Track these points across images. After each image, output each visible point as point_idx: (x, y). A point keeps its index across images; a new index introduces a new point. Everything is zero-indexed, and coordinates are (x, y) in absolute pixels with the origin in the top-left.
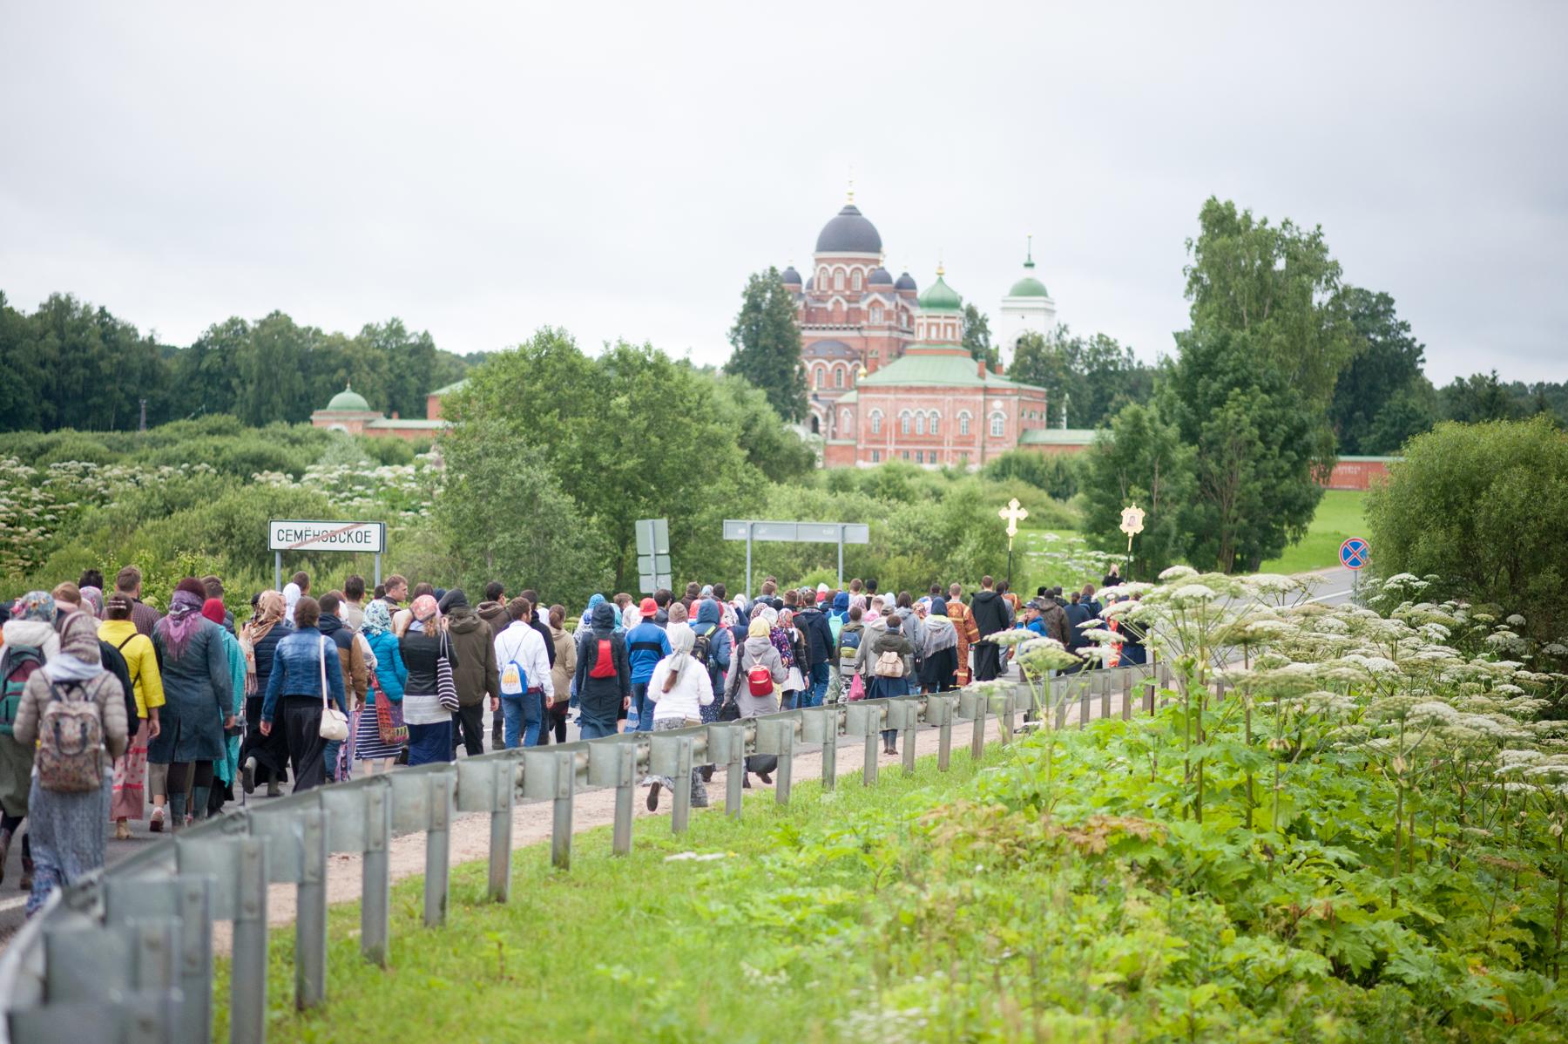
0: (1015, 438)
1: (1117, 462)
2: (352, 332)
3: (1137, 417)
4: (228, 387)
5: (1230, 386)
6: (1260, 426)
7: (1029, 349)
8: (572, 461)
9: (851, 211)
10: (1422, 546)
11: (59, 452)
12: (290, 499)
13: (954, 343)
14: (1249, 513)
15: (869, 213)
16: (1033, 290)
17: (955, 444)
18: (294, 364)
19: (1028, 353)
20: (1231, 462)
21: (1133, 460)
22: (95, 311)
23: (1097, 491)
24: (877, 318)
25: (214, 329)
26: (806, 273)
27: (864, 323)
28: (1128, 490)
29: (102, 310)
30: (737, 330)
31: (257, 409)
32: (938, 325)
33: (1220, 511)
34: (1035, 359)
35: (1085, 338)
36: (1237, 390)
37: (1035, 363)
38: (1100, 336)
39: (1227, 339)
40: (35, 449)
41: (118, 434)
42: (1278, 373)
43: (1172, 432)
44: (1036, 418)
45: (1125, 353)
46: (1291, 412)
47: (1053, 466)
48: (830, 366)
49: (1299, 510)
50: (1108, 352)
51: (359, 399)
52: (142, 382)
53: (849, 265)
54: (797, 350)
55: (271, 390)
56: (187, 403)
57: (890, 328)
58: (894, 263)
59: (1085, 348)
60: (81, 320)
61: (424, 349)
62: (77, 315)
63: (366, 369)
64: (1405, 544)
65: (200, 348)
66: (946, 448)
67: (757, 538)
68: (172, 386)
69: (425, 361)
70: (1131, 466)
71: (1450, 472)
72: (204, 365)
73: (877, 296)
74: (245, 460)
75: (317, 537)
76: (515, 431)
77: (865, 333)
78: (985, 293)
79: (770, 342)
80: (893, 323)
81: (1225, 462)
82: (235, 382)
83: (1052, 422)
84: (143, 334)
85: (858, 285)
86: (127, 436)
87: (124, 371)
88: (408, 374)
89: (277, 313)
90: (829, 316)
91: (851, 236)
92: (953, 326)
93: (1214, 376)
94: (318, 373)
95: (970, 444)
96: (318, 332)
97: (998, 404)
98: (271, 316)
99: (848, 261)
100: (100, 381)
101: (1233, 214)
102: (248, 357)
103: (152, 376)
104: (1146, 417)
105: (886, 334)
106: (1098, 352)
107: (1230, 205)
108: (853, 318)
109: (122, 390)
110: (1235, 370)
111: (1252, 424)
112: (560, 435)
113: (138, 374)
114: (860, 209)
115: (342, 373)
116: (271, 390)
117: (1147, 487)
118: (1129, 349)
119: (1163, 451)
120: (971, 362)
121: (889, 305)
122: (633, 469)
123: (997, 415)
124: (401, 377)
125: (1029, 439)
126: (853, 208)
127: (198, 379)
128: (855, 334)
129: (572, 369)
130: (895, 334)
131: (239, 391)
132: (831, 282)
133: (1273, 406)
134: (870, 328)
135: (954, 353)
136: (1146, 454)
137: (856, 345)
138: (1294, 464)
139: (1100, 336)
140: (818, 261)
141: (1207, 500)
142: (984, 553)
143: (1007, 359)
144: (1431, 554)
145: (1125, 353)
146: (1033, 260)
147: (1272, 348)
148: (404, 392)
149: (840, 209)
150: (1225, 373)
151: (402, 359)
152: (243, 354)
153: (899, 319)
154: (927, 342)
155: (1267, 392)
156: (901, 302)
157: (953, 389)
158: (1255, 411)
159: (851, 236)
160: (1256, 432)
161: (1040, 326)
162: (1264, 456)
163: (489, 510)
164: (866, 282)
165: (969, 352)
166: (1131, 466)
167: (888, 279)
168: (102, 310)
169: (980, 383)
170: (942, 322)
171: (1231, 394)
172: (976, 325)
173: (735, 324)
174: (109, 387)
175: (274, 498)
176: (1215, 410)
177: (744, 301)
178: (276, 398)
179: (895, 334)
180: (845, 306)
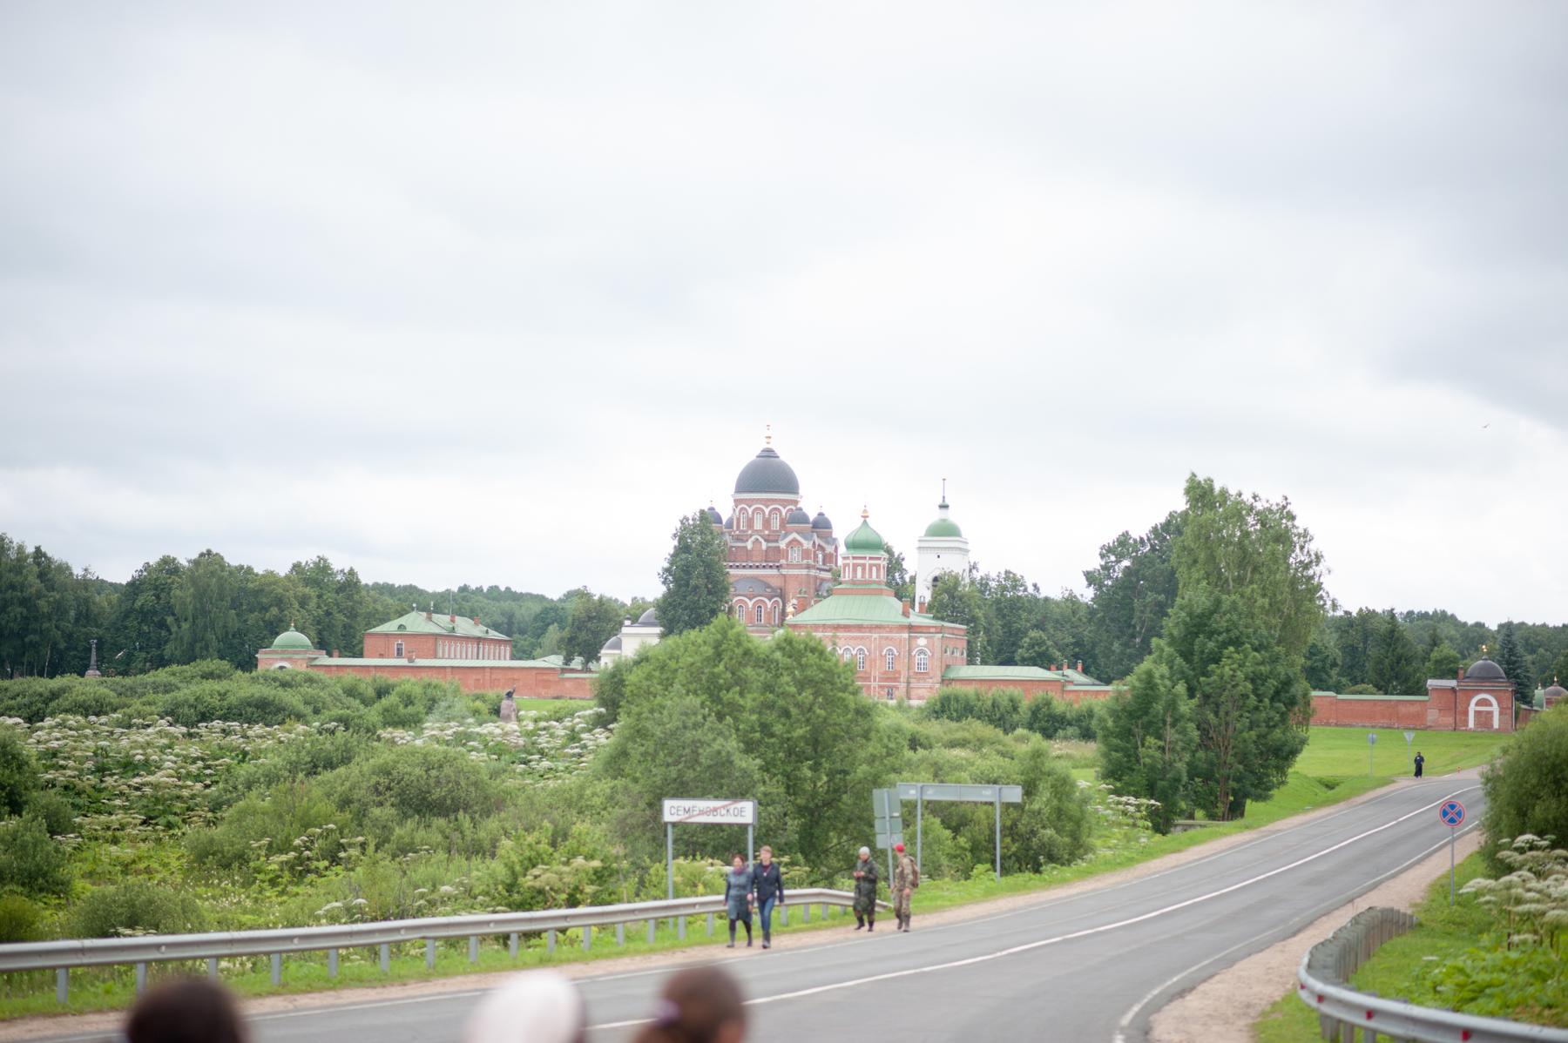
0: (939, 674)
1: (1131, 715)
2: (283, 570)
3: (1150, 674)
4: (162, 625)
5: (1225, 645)
6: (1253, 681)
7: (945, 587)
8: (753, 730)
9: (769, 454)
10: (1538, 812)
11: (64, 702)
12: (441, 757)
13: (879, 583)
14: (1243, 758)
15: (786, 456)
16: (945, 530)
17: (881, 680)
18: (227, 603)
19: (947, 591)
20: (1227, 713)
21: (1146, 713)
22: (30, 550)
23: (1115, 741)
24: (795, 556)
25: (147, 566)
26: (726, 511)
27: (783, 562)
28: (1143, 740)
29: (38, 549)
30: (667, 570)
31: (192, 646)
32: (863, 566)
33: (1218, 757)
34: (952, 597)
35: (993, 575)
36: (1232, 649)
37: (950, 600)
38: (1007, 572)
39: (1218, 602)
40: (47, 694)
41: (118, 679)
42: (1265, 633)
43: (1181, 688)
44: (957, 654)
45: (1031, 590)
46: (1280, 669)
47: (989, 703)
48: (750, 604)
49: (1284, 754)
50: (1014, 587)
51: (302, 638)
52: (77, 620)
53: (767, 505)
54: (726, 590)
55: (205, 628)
56: (122, 640)
57: (808, 567)
58: (810, 506)
59: (993, 584)
60: (18, 560)
61: (350, 584)
62: (13, 555)
63: (296, 606)
64: (1522, 813)
65: (135, 587)
66: (873, 684)
67: (926, 798)
68: (106, 624)
69: (350, 597)
70: (1145, 719)
71: (1557, 755)
72: (138, 604)
73: (795, 535)
74: (249, 705)
75: (702, 813)
76: (703, 705)
77: (784, 571)
78: (904, 538)
79: (701, 582)
80: (811, 562)
81: (1222, 713)
82: (170, 619)
83: (971, 662)
84: (78, 571)
85: (776, 525)
86: (128, 681)
87: (59, 609)
88: (335, 611)
89: (209, 552)
90: (748, 554)
91: (768, 477)
92: (878, 567)
93: (1211, 634)
94: (251, 611)
95: (896, 679)
96: (250, 570)
97: (922, 641)
98: (202, 555)
99: (766, 502)
100: (36, 619)
101: (1211, 489)
102: (182, 595)
103: (86, 615)
104: (1157, 675)
105: (804, 572)
106: (1004, 588)
107: (1210, 481)
108: (773, 557)
109: (57, 627)
110: (1228, 631)
111: (1246, 679)
112: (741, 709)
113: (72, 613)
114: (778, 451)
115: (274, 611)
116: (205, 628)
117: (1159, 737)
118: (1035, 586)
119: (1172, 705)
120: (894, 600)
121: (807, 545)
122: (802, 737)
123: (921, 652)
124: (328, 614)
125: (952, 675)
126: (770, 451)
127: (133, 616)
128: (775, 572)
129: (747, 653)
130: (813, 572)
131: (174, 629)
132: (750, 522)
133: (1262, 663)
134: (789, 566)
135: (879, 592)
136: (1159, 707)
137: (775, 583)
138: (1282, 714)
139: (1007, 572)
140: (737, 502)
141: (1207, 748)
142: (1055, 802)
143: (924, 593)
144: (1546, 820)
145: (1031, 590)
146: (947, 502)
147: (1256, 611)
148: (330, 626)
149: (758, 452)
150: (1220, 633)
151: (330, 597)
152: (178, 592)
153: (816, 556)
154: (853, 582)
155: (1256, 650)
156: (818, 541)
157: (879, 627)
158: (1249, 668)
159: (768, 477)
160: (1250, 686)
161: (954, 564)
162: (1257, 708)
163: (690, 774)
164: (783, 523)
165: (892, 591)
166: (1145, 719)
167: (803, 519)
168: (38, 549)
169: (906, 621)
170: (868, 562)
171: (1225, 652)
172: (895, 565)
173: (666, 565)
174: (45, 625)
175: (425, 755)
176: (1212, 667)
177: (676, 543)
178: (210, 636)
179: (813, 572)
180: (764, 545)
